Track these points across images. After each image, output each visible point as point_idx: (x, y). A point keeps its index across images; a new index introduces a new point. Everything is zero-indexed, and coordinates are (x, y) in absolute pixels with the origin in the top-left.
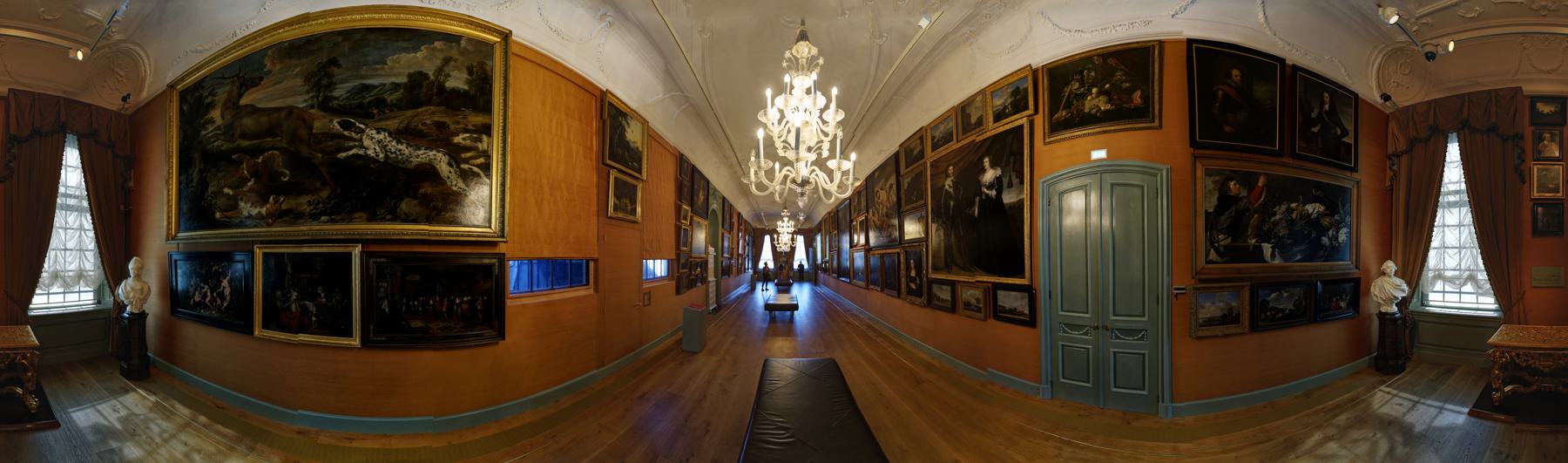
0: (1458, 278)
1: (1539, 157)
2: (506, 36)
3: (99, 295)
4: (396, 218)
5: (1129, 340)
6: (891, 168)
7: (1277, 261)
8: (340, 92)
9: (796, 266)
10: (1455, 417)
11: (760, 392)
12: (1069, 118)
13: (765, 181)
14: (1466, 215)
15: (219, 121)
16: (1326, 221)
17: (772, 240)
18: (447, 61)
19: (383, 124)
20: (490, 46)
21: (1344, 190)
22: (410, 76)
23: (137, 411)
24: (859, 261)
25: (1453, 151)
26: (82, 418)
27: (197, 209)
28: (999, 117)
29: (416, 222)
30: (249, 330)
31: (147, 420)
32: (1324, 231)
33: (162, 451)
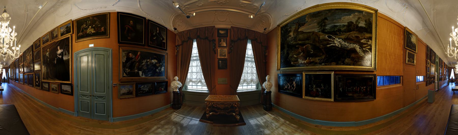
0: (196, 81)
1: (220, 47)
2: (376, 11)
3: (257, 86)
4: (344, 64)
5: (100, 99)
6: (31, 49)
7: (144, 76)
8: (328, 27)
9: (3, 78)
10: (195, 122)
11: (451, 114)
12: (82, 35)
13: (452, 53)
14: (199, 63)
15: (292, 36)
16: (158, 65)
17: (454, 70)
18: (359, 18)
19: (340, 37)
20: (372, 14)
21: (163, 56)
22: (348, 23)
23: (268, 120)
24: (21, 76)
25: (195, 44)
26: (253, 122)
27: (286, 61)
28: (62, 34)
29: (350, 65)
30: (301, 96)
31: (271, 123)
32: (157, 68)
33: (276, 131)
